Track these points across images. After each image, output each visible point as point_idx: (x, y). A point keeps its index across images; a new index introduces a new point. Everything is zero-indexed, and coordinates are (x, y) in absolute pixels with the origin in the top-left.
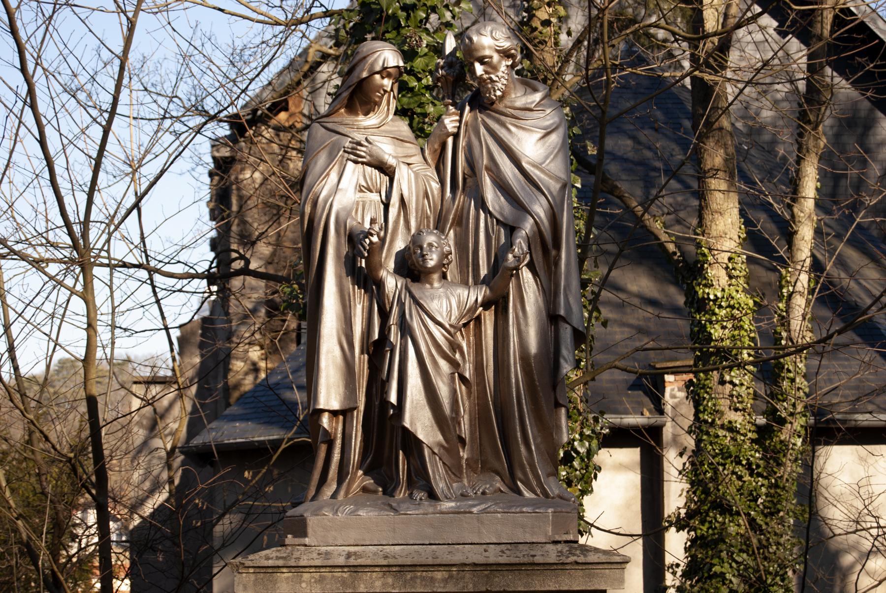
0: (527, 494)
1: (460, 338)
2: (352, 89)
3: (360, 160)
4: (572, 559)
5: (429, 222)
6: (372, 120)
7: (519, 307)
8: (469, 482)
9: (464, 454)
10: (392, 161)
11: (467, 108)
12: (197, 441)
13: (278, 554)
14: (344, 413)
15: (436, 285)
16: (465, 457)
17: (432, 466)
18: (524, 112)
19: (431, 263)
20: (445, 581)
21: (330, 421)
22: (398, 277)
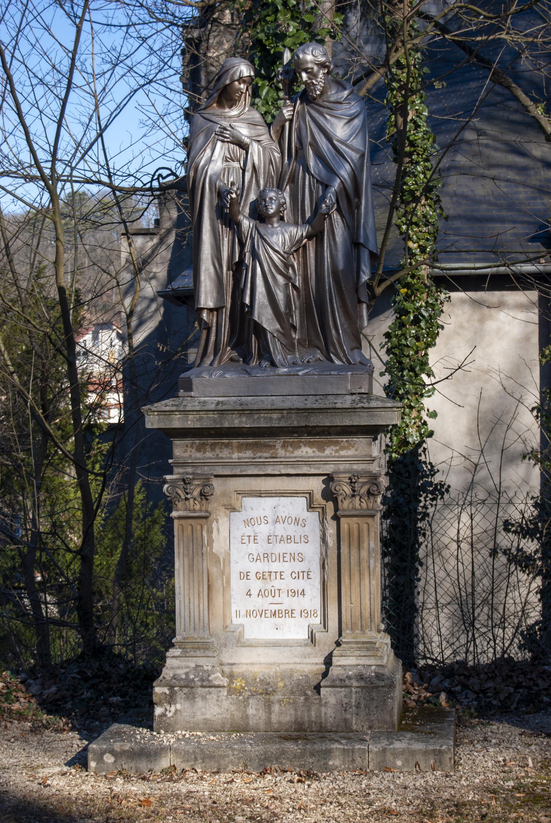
0: (337, 362)
1: (293, 260)
2: (219, 92)
3: (226, 140)
4: (360, 405)
5: (273, 180)
6: (234, 112)
7: (331, 238)
8: (299, 354)
9: (296, 336)
10: (247, 140)
11: (298, 102)
12: (175, 285)
13: (173, 403)
14: (217, 310)
15: (276, 225)
16: (297, 338)
17: (273, 345)
18: (336, 105)
19: (271, 211)
20: (279, 419)
21: (208, 315)
22: (251, 220)
